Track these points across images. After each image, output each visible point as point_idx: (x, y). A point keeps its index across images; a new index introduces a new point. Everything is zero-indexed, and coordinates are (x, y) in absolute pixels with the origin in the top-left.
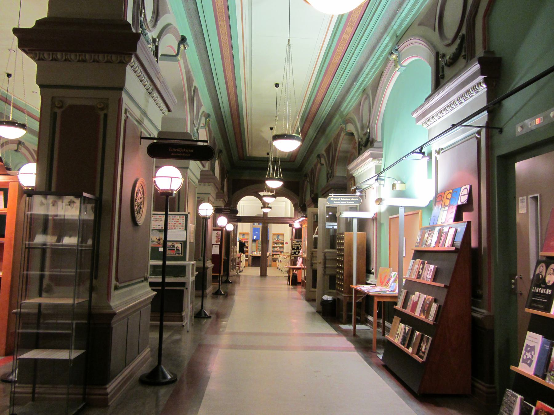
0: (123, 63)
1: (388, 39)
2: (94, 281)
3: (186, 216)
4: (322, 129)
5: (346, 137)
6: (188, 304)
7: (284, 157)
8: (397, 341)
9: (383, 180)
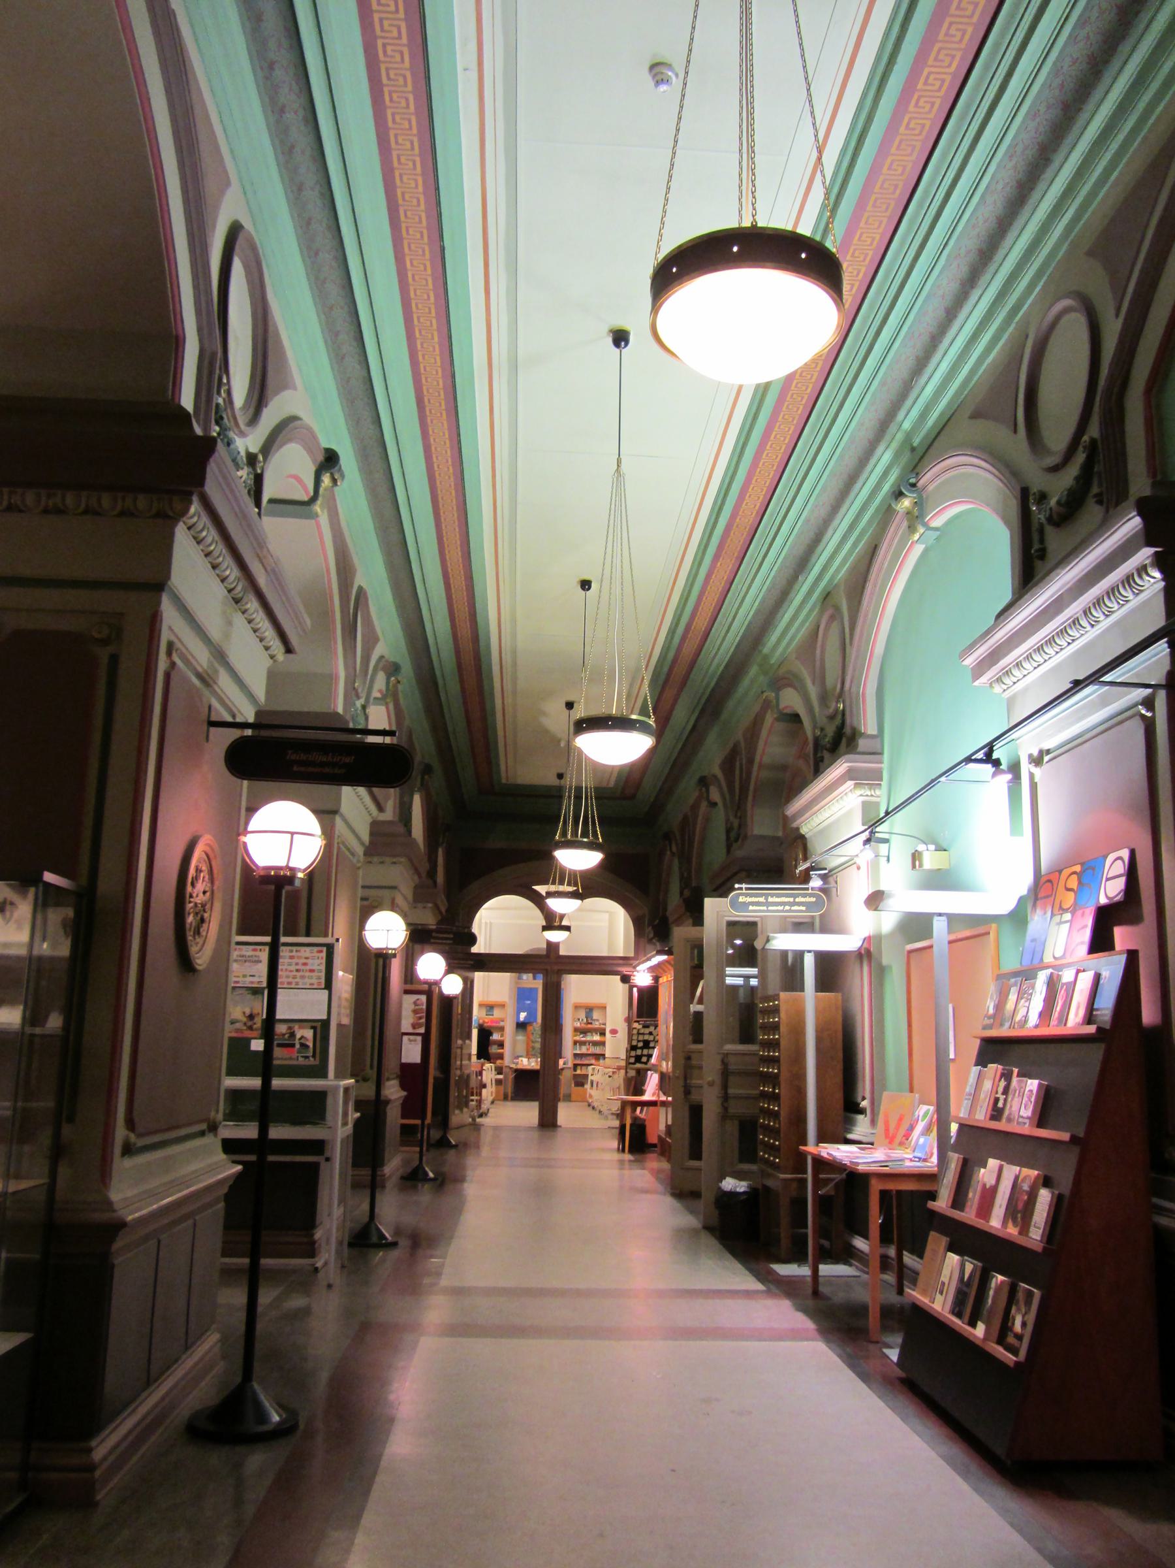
0: (167, 517)
1: (887, 457)
2: (67, 1131)
3: (330, 949)
5: (780, 726)
6: (330, 1206)
7: (604, 785)
8: (940, 1305)
9: (886, 841)
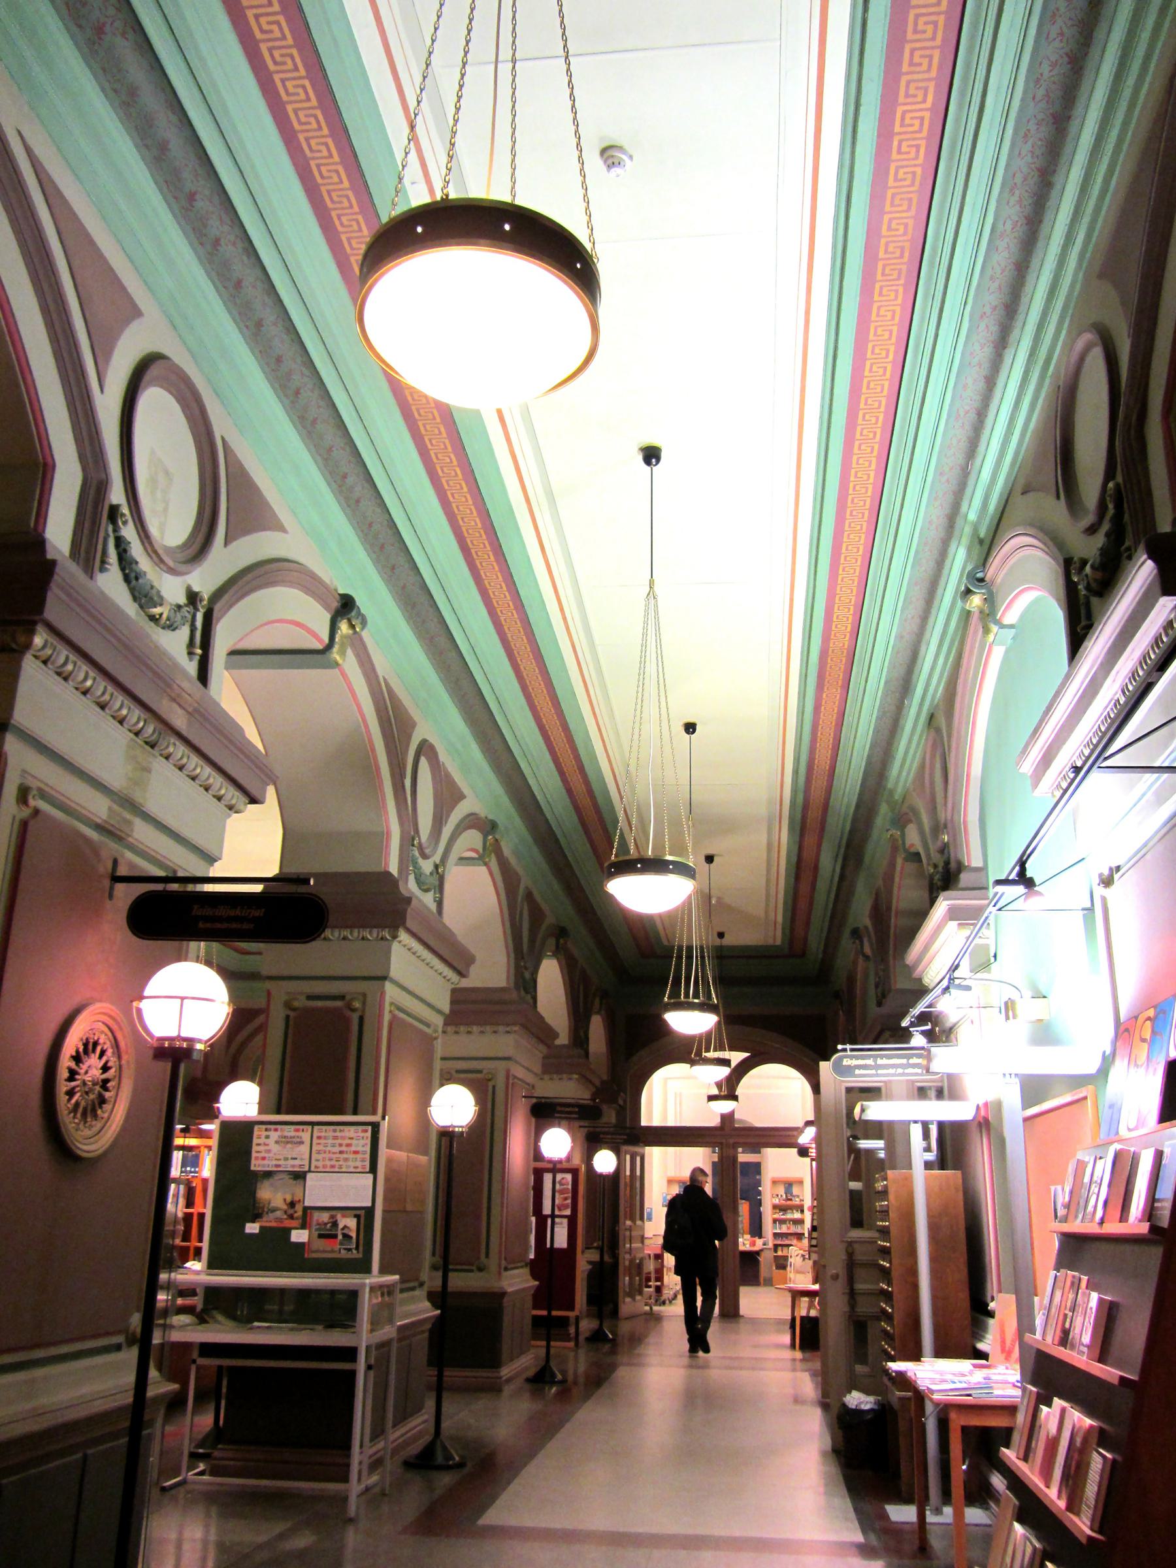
0: (13, 650)
3: (375, 1127)
4: (853, 850)
